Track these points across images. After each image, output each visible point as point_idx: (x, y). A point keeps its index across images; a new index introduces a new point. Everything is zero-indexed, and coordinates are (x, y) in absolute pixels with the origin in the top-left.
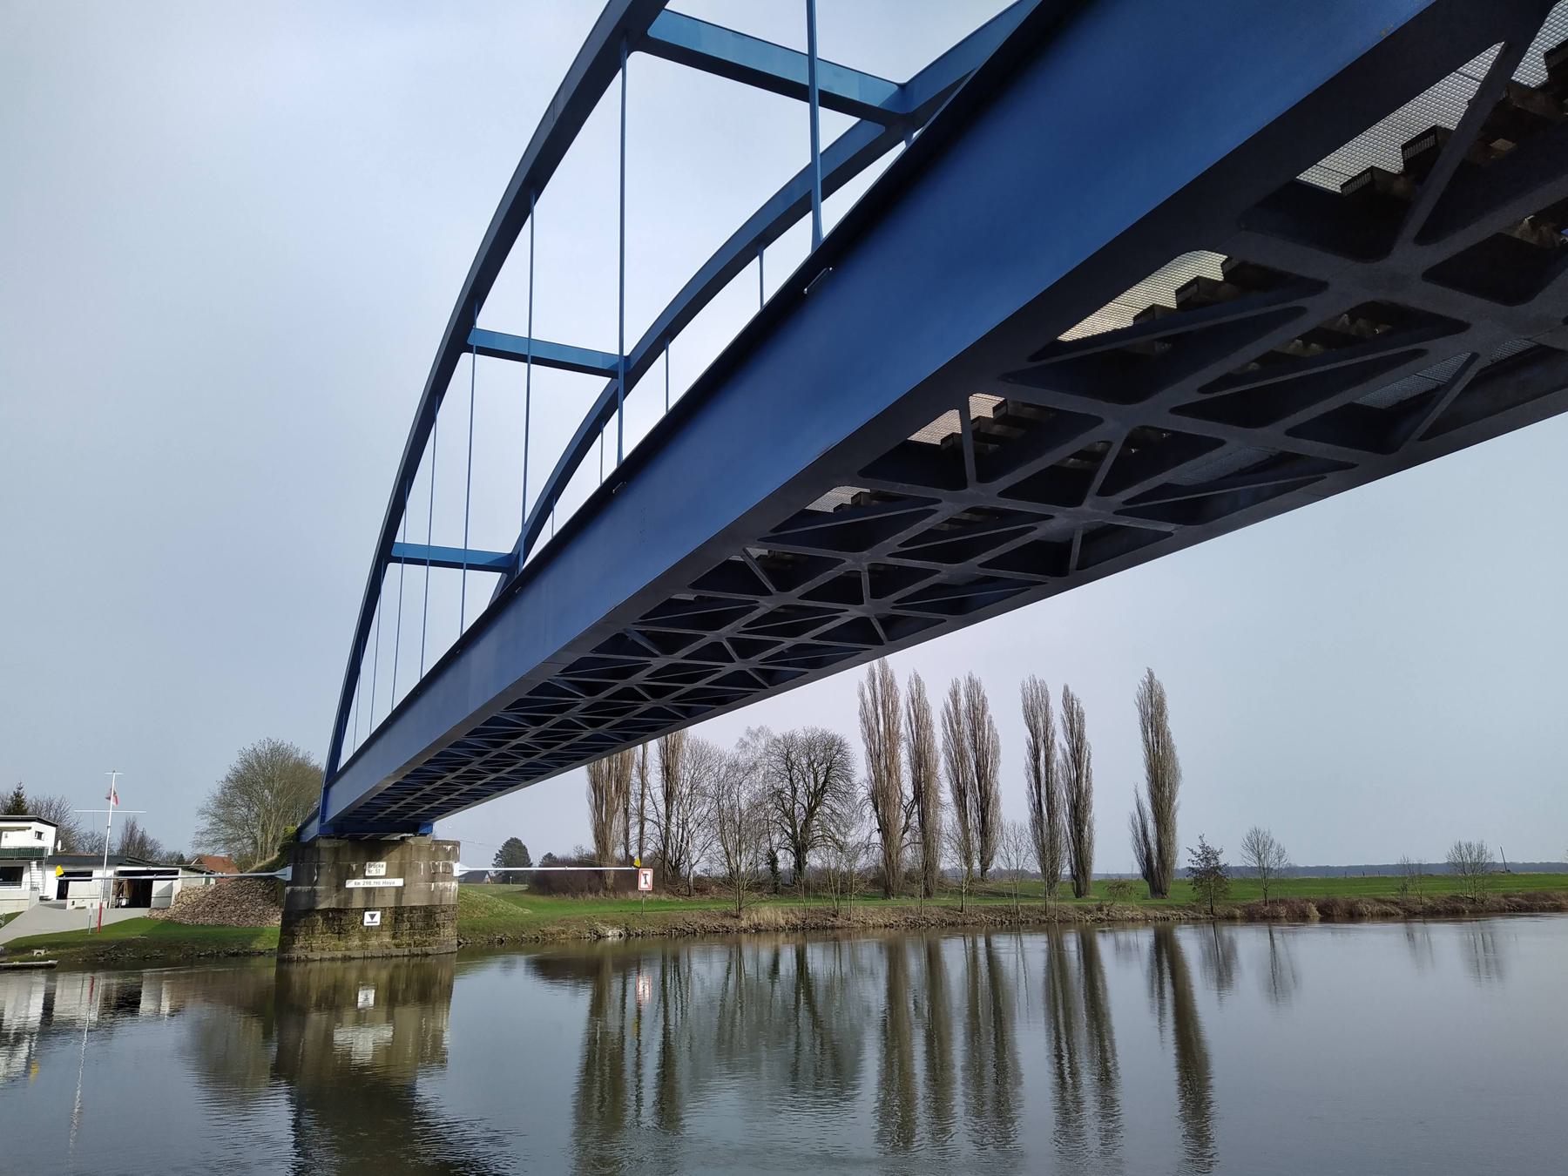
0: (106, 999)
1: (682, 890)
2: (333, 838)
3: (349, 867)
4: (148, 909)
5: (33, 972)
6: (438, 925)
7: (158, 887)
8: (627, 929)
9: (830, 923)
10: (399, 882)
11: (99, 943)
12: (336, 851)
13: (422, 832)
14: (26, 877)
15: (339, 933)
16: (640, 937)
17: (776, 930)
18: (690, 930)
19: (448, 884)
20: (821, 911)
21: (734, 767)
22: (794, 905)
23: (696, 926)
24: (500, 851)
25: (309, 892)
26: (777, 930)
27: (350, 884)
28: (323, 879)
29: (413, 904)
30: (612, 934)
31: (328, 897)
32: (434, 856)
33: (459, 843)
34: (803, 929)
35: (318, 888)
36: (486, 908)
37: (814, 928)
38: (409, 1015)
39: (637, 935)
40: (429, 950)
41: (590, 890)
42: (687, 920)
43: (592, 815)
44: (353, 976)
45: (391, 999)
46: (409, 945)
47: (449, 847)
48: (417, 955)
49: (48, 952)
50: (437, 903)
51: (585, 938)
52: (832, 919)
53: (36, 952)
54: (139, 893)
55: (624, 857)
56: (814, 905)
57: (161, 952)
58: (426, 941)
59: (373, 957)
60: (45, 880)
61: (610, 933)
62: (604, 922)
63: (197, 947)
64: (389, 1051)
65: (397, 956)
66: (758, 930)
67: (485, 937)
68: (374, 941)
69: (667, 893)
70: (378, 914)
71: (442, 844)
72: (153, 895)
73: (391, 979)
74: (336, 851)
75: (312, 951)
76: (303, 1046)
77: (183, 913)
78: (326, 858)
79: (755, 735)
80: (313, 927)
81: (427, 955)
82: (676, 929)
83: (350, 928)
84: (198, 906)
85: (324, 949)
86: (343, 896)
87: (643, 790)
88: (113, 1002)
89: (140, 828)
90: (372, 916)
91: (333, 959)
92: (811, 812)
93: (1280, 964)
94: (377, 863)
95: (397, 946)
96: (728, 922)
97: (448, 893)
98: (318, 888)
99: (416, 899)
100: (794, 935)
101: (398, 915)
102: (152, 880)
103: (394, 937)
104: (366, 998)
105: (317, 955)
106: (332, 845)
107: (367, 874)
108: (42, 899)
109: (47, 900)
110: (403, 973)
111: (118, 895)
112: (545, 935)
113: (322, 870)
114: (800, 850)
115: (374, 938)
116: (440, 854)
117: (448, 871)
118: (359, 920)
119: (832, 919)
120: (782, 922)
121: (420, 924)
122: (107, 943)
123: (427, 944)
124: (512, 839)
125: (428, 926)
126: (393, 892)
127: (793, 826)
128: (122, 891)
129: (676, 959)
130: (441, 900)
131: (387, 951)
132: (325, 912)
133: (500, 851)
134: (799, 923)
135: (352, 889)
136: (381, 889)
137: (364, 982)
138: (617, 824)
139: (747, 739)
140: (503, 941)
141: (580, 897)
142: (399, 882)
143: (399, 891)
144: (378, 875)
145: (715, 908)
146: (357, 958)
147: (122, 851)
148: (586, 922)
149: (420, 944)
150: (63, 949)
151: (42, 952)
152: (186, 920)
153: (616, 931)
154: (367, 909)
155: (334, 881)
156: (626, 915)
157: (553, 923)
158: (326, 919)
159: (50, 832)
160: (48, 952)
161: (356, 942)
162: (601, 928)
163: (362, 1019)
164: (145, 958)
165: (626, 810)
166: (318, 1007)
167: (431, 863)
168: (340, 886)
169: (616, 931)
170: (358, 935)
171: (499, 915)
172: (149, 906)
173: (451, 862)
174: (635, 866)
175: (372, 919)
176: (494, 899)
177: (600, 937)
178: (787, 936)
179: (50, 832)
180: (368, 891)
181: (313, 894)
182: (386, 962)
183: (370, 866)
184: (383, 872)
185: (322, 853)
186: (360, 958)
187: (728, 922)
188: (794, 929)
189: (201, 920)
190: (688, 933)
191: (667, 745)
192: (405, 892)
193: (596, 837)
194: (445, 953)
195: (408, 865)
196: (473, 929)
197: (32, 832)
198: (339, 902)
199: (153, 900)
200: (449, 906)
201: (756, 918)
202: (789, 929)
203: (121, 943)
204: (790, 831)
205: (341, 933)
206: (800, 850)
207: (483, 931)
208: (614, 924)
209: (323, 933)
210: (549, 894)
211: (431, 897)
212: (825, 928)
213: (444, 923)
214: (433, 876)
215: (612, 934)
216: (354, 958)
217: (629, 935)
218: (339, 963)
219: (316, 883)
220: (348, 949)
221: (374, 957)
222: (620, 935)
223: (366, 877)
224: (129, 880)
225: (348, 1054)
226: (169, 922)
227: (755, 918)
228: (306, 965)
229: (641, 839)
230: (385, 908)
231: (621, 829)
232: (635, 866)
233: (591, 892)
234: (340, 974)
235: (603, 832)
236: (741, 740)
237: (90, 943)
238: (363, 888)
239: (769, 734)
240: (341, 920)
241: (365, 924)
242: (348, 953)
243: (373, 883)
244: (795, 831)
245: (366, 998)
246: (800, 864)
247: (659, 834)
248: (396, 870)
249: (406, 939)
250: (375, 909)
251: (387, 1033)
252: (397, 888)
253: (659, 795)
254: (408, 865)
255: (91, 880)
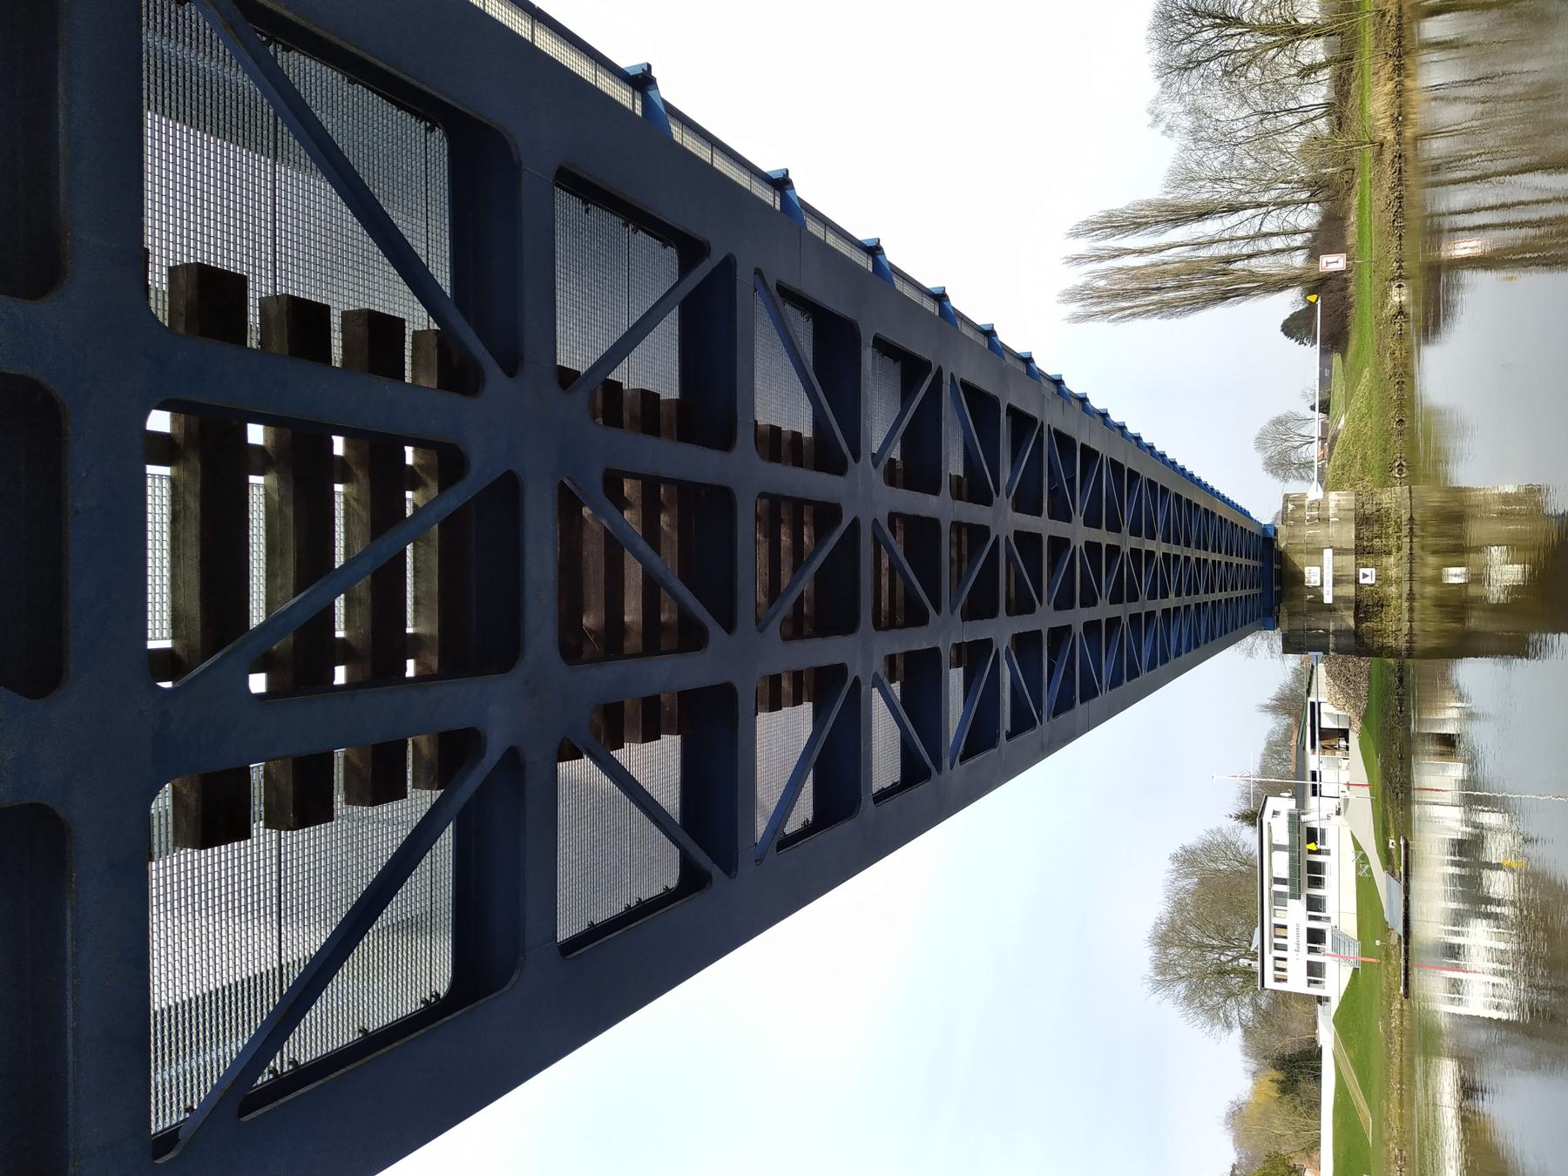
0: (1442, 754)
1: (1346, 177)
2: (1278, 617)
3: (1310, 601)
4: (1350, 732)
5: (1410, 873)
6: (1378, 510)
7: (1327, 723)
8: (1393, 279)
9: (1394, 20)
10: (1328, 553)
11: (1384, 794)
12: (1292, 614)
13: (1272, 534)
14: (1314, 825)
15: (1382, 606)
16: (1403, 264)
17: (1400, 94)
18: (1396, 203)
19: (1332, 504)
20: (1377, 32)
21: (1195, 134)
22: (1369, 68)
23: (1392, 197)
24: (1297, 341)
25: (1336, 636)
26: (1400, 92)
27: (1328, 599)
28: (1322, 624)
29: (1353, 537)
30: (1398, 296)
31: (1342, 618)
32: (1300, 522)
33: (1284, 496)
34: (1400, 56)
35: (1332, 628)
36: (1361, 421)
37: (1399, 43)
38: (1476, 531)
39: (1400, 267)
40: (1405, 517)
41: (1344, 289)
42: (1383, 208)
43: (1255, 298)
44: (1430, 590)
45: (1458, 551)
46: (1399, 538)
47: (1290, 506)
48: (1411, 529)
49: (1392, 836)
50: (1353, 514)
51: (1401, 330)
52: (1388, 18)
53: (1391, 846)
54: (1332, 738)
55: (1306, 251)
56: (1368, 40)
57: (1395, 744)
58: (1395, 521)
59: (1411, 573)
60: (1317, 812)
61: (1397, 299)
62: (1382, 308)
63: (1391, 713)
64: (1516, 548)
65: (1411, 549)
66: (1399, 119)
67: (1394, 438)
68: (1393, 573)
69: (1349, 195)
70: (1362, 571)
71: (1287, 515)
72: (1336, 727)
73: (1435, 552)
74: (1292, 614)
75: (1401, 630)
76: (1508, 632)
77: (1355, 706)
78: (1299, 623)
79: (1157, 118)
80: (1374, 630)
81: (1411, 519)
82: (1394, 221)
83: (1376, 596)
84: (1348, 693)
85: (1399, 619)
86: (1342, 605)
87: (1226, 240)
88: (1444, 749)
89: (1268, 702)
90: (1365, 576)
91: (1411, 610)
92: (1253, 28)
93: (1433, 1088)
94: (1306, 575)
95: (1399, 549)
96: (1388, 156)
97: (1342, 502)
98: (1332, 628)
99: (1348, 536)
100: (1407, 66)
101: (1363, 551)
102: (1320, 728)
103: (1390, 553)
104: (1455, 575)
105: (1405, 626)
106: (1286, 619)
107: (1318, 584)
108: (1338, 813)
109: (1339, 809)
110: (1430, 541)
111: (1336, 749)
112: (1395, 374)
113: (1313, 626)
114: (1298, 32)
115: (1390, 573)
116: (1297, 515)
117: (1319, 505)
118: (1369, 588)
119: (1388, 18)
120: (1390, 85)
121: (1376, 528)
122: (1384, 788)
123: (1398, 520)
124: (1283, 330)
125: (1379, 520)
126: (1339, 558)
127: (1266, 48)
128: (1332, 746)
129: (1436, 169)
130: (1349, 510)
131: (1405, 559)
132: (1358, 620)
133: (1297, 341)
134: (1391, 63)
135: (1335, 598)
136: (1335, 569)
137: (1437, 580)
138: (1260, 265)
139: (1162, 126)
140: (1401, 420)
141: (1351, 300)
142: (1328, 553)
143: (1338, 552)
144: (1320, 575)
145: (1370, 172)
146: (1411, 587)
147: (1290, 714)
148: (1381, 327)
149: (1398, 527)
150: (1389, 824)
151: (1391, 841)
152: (1363, 705)
153: (1395, 291)
154: (1357, 581)
155: (1324, 615)
156: (1376, 280)
157: (1382, 363)
158: (1366, 619)
159: (1273, 803)
160: (1392, 836)
161: (1393, 590)
162: (1390, 310)
163: (1478, 578)
164: (1401, 758)
165: (1250, 256)
166: (1462, 620)
167: (1307, 524)
168: (1330, 609)
169: (1395, 291)
170: (1385, 588)
171: (1369, 407)
172: (1347, 730)
173: (1307, 503)
174: (1317, 300)
175: (1368, 576)
176: (1352, 407)
177: (1401, 312)
178: (1407, 76)
179: (1273, 803)
180: (1337, 581)
181: (1337, 633)
182: (1417, 560)
183: (1309, 582)
184: (1317, 570)
185: (1294, 628)
186: (1411, 584)
187: (1388, 156)
188: (1399, 69)
189: (1363, 693)
190: (1400, 207)
191: (1171, 220)
192: (1339, 546)
193: (1281, 290)
194: (1411, 500)
195: (1309, 546)
196: (1385, 450)
197: (1272, 821)
198: (1348, 608)
199: (1341, 727)
200: (1357, 500)
201: (1382, 121)
202: (1399, 75)
203: (1385, 777)
204: (1272, 53)
205: (1381, 604)
206: (1298, 32)
207: (1387, 441)
208: (1385, 294)
209: (1382, 620)
210: (1348, 333)
211: (1348, 520)
212: (1399, 27)
213: (1376, 504)
214: (1323, 520)
215: (1398, 296)
216: (1411, 590)
217: (1400, 276)
218: (1415, 604)
219: (1327, 631)
220: (1400, 597)
221: (1411, 570)
222: (1400, 286)
223: (1322, 585)
224: (1320, 739)
225: (1514, 589)
226: (1364, 719)
227: (1384, 121)
228: (1415, 635)
229: (1285, 234)
230: (1356, 565)
231: (1271, 259)
232: (1317, 300)
233: (1347, 288)
234: (1428, 603)
235: (1275, 284)
236: (1164, 133)
237: (1385, 802)
238: (1334, 586)
239: (1157, 100)
240: (1367, 605)
241: (1373, 582)
242: (1405, 596)
243: (1329, 579)
244: (1272, 45)
245: (1455, 575)
246: (1314, 31)
247: (1278, 211)
248: (1315, 557)
249: (1392, 542)
250: (1357, 574)
251: (1496, 553)
252: (1334, 554)
253: (1234, 219)
254: (1309, 546)
255: (1320, 772)
